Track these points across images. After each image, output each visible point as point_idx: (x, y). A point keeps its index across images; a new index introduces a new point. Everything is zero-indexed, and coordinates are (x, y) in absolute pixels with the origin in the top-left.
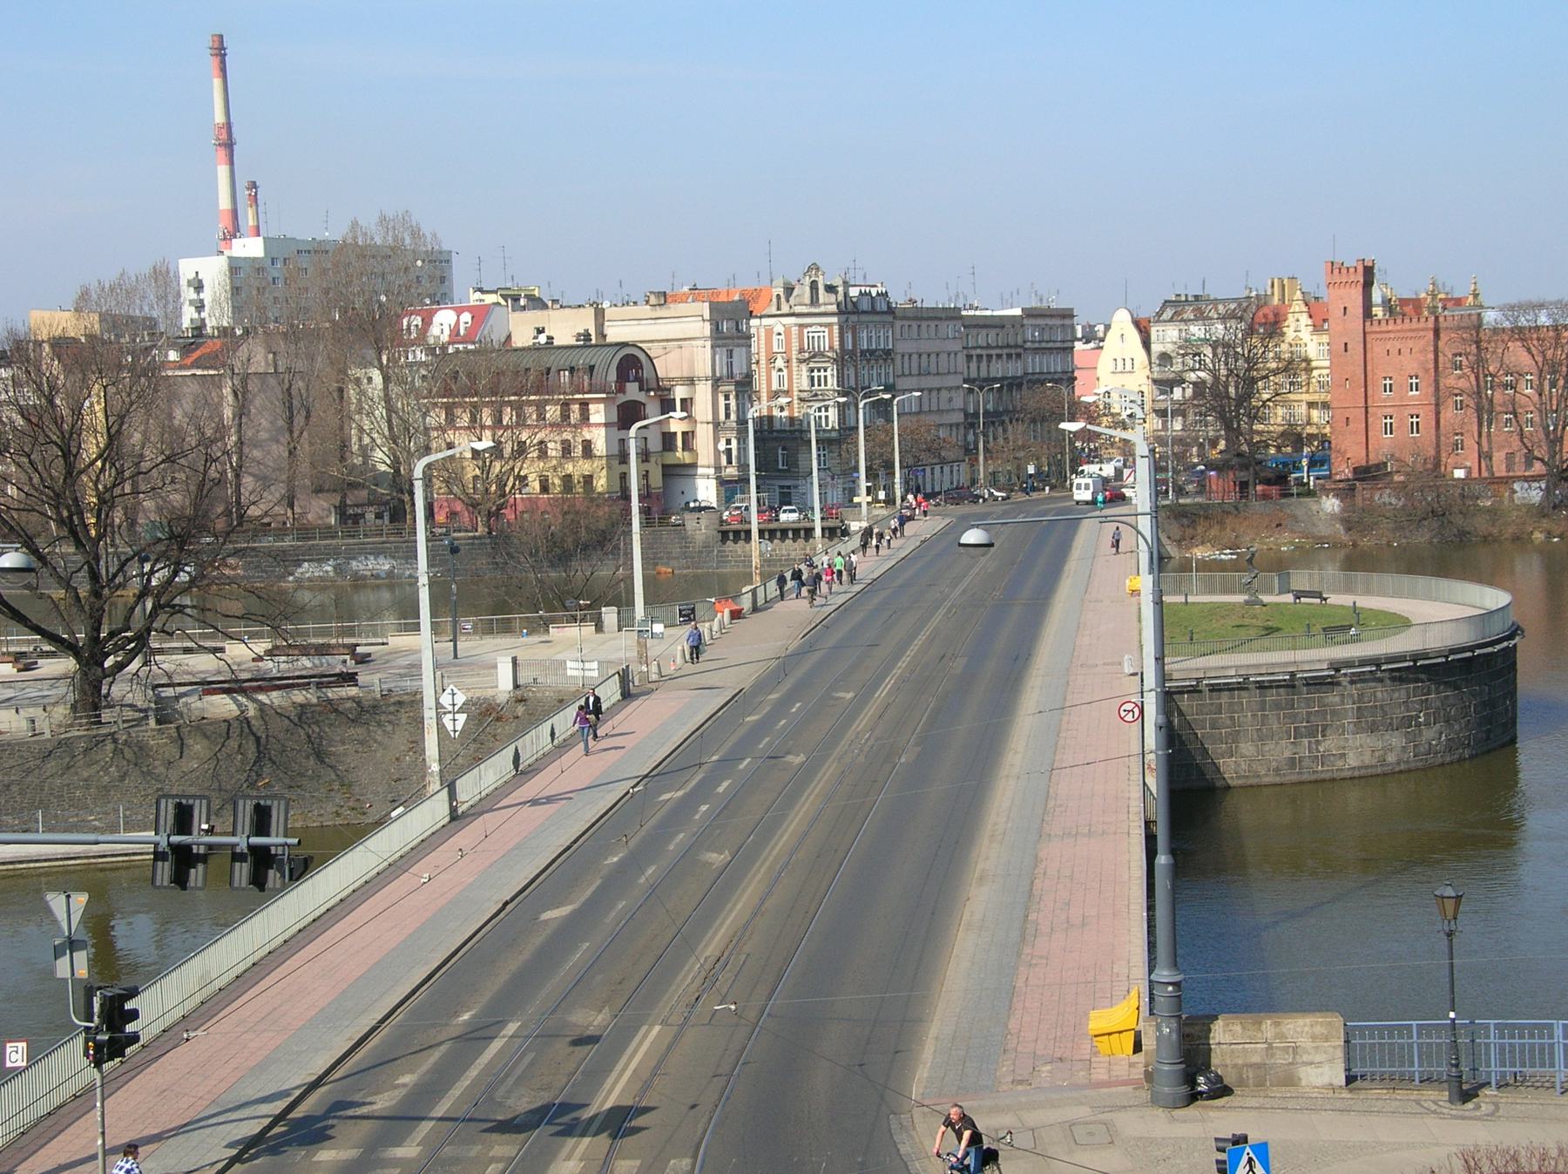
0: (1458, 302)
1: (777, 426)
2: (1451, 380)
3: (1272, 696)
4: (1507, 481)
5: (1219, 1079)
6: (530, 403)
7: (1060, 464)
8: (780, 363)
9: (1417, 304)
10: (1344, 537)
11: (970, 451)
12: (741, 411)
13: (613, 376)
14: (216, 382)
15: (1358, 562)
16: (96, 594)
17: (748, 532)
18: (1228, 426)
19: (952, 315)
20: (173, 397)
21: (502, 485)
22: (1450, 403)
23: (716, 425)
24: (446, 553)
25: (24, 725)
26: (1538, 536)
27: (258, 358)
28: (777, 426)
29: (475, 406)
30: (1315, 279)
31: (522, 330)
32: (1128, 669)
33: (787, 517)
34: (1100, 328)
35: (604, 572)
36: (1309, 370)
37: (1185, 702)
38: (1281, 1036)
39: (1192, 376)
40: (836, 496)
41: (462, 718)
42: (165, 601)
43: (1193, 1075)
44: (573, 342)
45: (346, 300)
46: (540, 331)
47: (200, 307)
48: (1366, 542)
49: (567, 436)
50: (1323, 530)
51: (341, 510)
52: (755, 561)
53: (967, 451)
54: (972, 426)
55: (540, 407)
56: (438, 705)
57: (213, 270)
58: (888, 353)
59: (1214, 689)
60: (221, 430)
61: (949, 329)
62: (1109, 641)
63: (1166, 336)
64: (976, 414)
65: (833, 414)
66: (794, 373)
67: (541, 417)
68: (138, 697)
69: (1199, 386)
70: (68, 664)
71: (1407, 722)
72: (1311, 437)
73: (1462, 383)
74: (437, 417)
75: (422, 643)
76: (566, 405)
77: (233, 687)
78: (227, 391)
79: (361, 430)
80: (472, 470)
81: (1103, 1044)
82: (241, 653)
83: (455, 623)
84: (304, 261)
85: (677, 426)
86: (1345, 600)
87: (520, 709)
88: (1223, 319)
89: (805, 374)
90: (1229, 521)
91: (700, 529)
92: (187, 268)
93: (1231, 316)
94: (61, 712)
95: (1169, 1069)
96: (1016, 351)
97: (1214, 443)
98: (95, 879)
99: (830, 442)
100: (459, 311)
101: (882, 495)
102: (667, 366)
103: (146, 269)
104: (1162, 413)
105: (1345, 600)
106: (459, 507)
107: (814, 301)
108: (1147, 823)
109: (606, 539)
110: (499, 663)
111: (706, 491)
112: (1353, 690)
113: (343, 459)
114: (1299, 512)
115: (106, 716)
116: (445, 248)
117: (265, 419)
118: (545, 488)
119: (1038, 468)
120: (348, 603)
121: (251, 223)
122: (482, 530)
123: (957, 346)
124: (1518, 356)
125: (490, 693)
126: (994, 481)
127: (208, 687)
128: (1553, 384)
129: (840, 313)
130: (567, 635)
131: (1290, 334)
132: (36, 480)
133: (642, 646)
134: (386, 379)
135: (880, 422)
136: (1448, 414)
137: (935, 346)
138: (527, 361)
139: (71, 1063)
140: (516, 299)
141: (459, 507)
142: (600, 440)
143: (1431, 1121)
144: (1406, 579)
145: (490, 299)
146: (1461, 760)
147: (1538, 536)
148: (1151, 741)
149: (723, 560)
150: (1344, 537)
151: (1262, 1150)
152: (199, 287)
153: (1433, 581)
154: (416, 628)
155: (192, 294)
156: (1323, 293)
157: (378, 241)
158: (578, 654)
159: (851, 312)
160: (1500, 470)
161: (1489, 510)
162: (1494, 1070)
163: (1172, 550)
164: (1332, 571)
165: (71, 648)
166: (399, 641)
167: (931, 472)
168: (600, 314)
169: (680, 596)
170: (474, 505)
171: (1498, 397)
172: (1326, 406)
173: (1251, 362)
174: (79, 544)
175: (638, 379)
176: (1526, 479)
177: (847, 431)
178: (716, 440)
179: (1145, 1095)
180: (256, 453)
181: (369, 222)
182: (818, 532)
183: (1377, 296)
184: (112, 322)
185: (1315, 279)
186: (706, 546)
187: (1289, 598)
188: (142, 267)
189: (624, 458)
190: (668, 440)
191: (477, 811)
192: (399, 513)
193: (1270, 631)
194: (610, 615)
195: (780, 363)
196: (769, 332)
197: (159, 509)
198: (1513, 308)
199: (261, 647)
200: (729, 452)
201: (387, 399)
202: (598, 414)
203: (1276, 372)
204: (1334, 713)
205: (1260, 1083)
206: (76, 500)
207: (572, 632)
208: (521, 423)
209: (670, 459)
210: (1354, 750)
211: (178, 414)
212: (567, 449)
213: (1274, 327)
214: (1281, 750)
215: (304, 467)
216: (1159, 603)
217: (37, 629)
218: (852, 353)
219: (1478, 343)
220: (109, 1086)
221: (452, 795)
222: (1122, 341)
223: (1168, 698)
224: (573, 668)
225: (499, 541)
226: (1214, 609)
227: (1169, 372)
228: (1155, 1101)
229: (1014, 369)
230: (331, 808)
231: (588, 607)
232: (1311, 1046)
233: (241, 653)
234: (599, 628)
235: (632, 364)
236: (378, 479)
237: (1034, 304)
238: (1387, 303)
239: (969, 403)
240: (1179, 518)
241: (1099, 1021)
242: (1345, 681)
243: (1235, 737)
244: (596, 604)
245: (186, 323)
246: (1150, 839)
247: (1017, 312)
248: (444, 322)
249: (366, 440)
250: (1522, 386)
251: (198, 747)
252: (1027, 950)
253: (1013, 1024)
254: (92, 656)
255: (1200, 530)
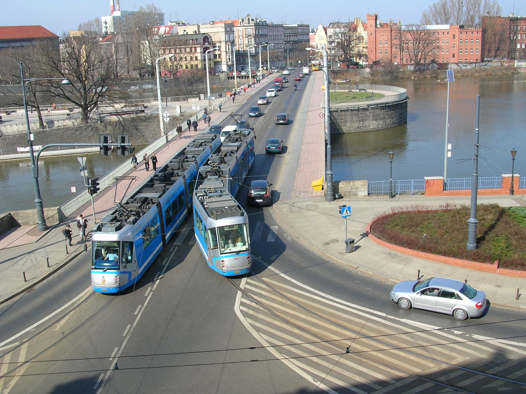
0: (396, 24)
1: (240, 52)
2: (395, 42)
3: (354, 112)
4: (406, 65)
5: (341, 195)
6: (183, 48)
7: (306, 61)
8: (241, 38)
9: (387, 25)
10: (370, 77)
11: (285, 58)
12: (232, 49)
13: (202, 41)
14: (111, 45)
15: (374, 83)
16: (85, 93)
17: (234, 77)
18: (345, 52)
19: (281, 26)
20: (101, 48)
21: (177, 67)
22: (394, 47)
23: (226, 52)
24: (164, 82)
25: (72, 123)
26: (413, 78)
27: (120, 39)
28: (240, 52)
29: (170, 49)
30: (364, 18)
31: (180, 31)
32: (322, 106)
33: (243, 73)
34: (315, 30)
35: (201, 87)
36: (363, 39)
37: (334, 114)
38: (354, 185)
39: (337, 41)
40: (254, 68)
41: (168, 119)
42: (101, 95)
43: (335, 194)
44: (192, 33)
45: (140, 25)
46: (185, 31)
47: (107, 28)
48: (375, 79)
49: (192, 55)
50: (366, 76)
51: (140, 74)
52: (236, 83)
53: (285, 58)
54: (286, 52)
55: (185, 49)
56: (163, 116)
57: (109, 19)
58: (266, 35)
59: (341, 111)
60: (112, 56)
61: (280, 29)
62: (317, 101)
63: (330, 31)
64: (287, 49)
65: (253, 49)
66: (244, 41)
67: (185, 51)
68: (96, 117)
69: (338, 43)
70: (80, 110)
71: (383, 118)
72: (363, 55)
73: (397, 43)
74: (161, 52)
75: (159, 103)
76: (191, 48)
77: (117, 114)
78: (113, 47)
79: (144, 55)
80: (170, 64)
81: (315, 188)
82: (118, 106)
83: (166, 99)
84: (130, 16)
85: (217, 53)
86: (371, 91)
87: (182, 118)
88: (343, 27)
89: (247, 40)
90: (345, 74)
91: (223, 76)
92: (103, 19)
93: (346, 27)
94: (79, 120)
95: (330, 193)
96: (296, 35)
97: (341, 56)
98: (90, 157)
99: (253, 56)
100: (166, 27)
101: (265, 68)
102: (214, 39)
103: (94, 19)
104: (329, 49)
105: (371, 91)
106: (167, 72)
107: (249, 23)
108: (326, 141)
109: (201, 79)
110: (177, 108)
111: (224, 68)
112: (372, 111)
113: (140, 62)
114: (361, 72)
115: (89, 121)
116: (162, 12)
117: (122, 54)
118: (187, 68)
119: (301, 62)
120: (142, 95)
121: (118, 8)
122: (172, 78)
123: (282, 34)
124: (409, 36)
125: (175, 114)
126: (291, 65)
127: (111, 114)
128: (416, 43)
129: (255, 26)
130: (193, 101)
131: (359, 31)
132: (71, 68)
133: (210, 102)
134: (149, 43)
135: (265, 51)
136: (394, 49)
137: (276, 33)
138: (182, 38)
139: (86, 195)
140: (179, 24)
141: (167, 72)
142: (199, 56)
143: (385, 202)
144: (384, 86)
145: (173, 24)
146: (395, 127)
147: (413, 78)
148: (326, 120)
149: (228, 84)
150: (370, 77)
151: (349, 208)
152: (106, 23)
153: (390, 87)
154: (158, 100)
155: (104, 25)
156: (366, 22)
157: (147, 11)
158: (195, 106)
159: (258, 25)
160: (405, 63)
161: (402, 72)
162: (399, 191)
163: (332, 80)
164: (368, 85)
165: (80, 106)
166: (154, 103)
167: (276, 61)
168: (199, 26)
169: (218, 92)
170: (170, 72)
171: (405, 46)
172: (367, 48)
173: (350, 37)
174: (81, 82)
175: (208, 42)
176: (410, 65)
177: (257, 53)
178: (226, 56)
179: (324, 199)
180: (120, 61)
181: (145, 6)
182: (250, 77)
183: (378, 23)
184: (87, 32)
185: (364, 18)
186: (225, 81)
187: (358, 91)
188: (93, 18)
189: (205, 60)
190: (215, 56)
191: (172, 140)
192: (153, 74)
193: (354, 98)
194: (202, 96)
195: (241, 38)
196: (238, 30)
197: (99, 74)
198: (407, 26)
199: (123, 105)
200: (229, 58)
201: (150, 48)
202: (199, 50)
203: (356, 39)
204: (368, 116)
205: (349, 196)
206: (80, 71)
207: (194, 100)
208: (181, 52)
209: (215, 60)
210: (372, 124)
211: (102, 52)
212: (191, 58)
213: (355, 29)
214: (356, 125)
215: (131, 63)
216: (329, 93)
217: (74, 102)
218: (258, 35)
219: (400, 33)
220: (95, 200)
221: (167, 137)
222: (320, 32)
223: (330, 112)
224: (194, 108)
225: (176, 80)
226: (341, 93)
227: (331, 40)
228: (326, 200)
229: (296, 39)
230: (140, 141)
231: (197, 94)
232: (360, 187)
233: (118, 106)
234: (200, 99)
235: (206, 38)
236: (148, 66)
237: (300, 23)
238: (380, 24)
239: (286, 46)
240: (333, 74)
241: (314, 183)
242: (370, 109)
243: (346, 122)
244: (199, 93)
245: (103, 32)
246: (326, 144)
247: (296, 25)
248: (162, 30)
249: (145, 57)
250: (409, 43)
251: (109, 128)
252: (298, 168)
253: (295, 185)
254: (85, 107)
255: (338, 76)
